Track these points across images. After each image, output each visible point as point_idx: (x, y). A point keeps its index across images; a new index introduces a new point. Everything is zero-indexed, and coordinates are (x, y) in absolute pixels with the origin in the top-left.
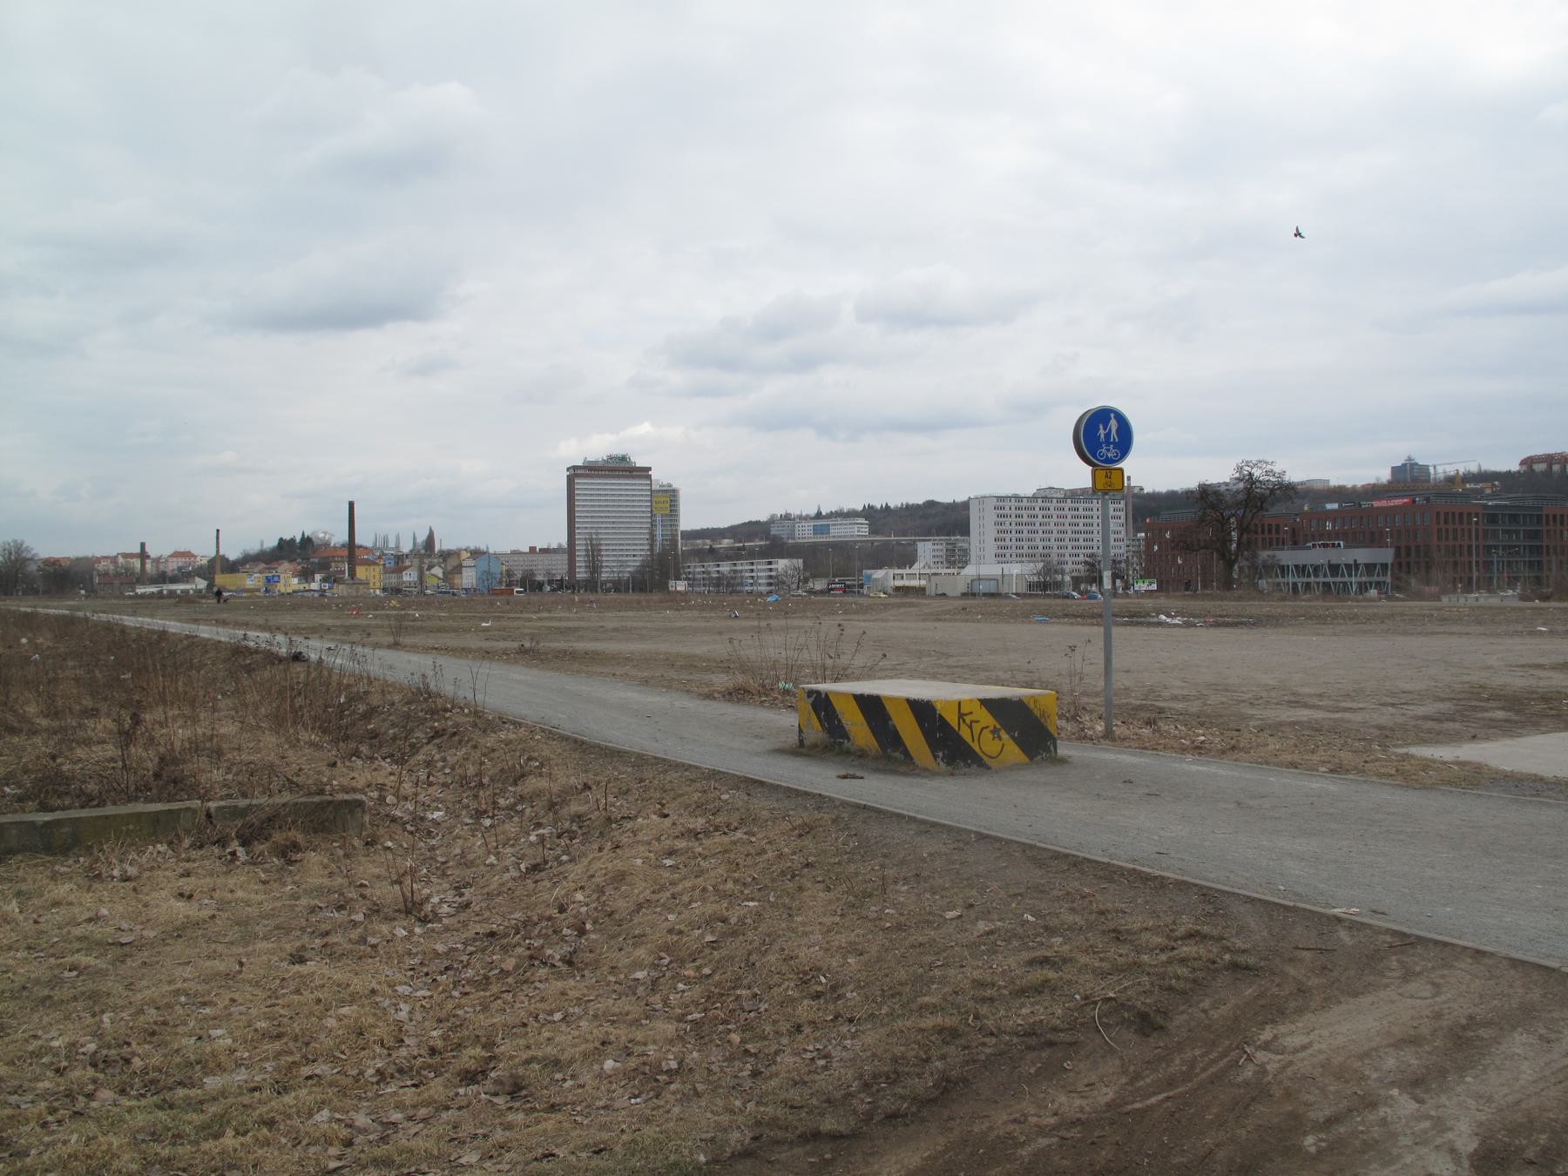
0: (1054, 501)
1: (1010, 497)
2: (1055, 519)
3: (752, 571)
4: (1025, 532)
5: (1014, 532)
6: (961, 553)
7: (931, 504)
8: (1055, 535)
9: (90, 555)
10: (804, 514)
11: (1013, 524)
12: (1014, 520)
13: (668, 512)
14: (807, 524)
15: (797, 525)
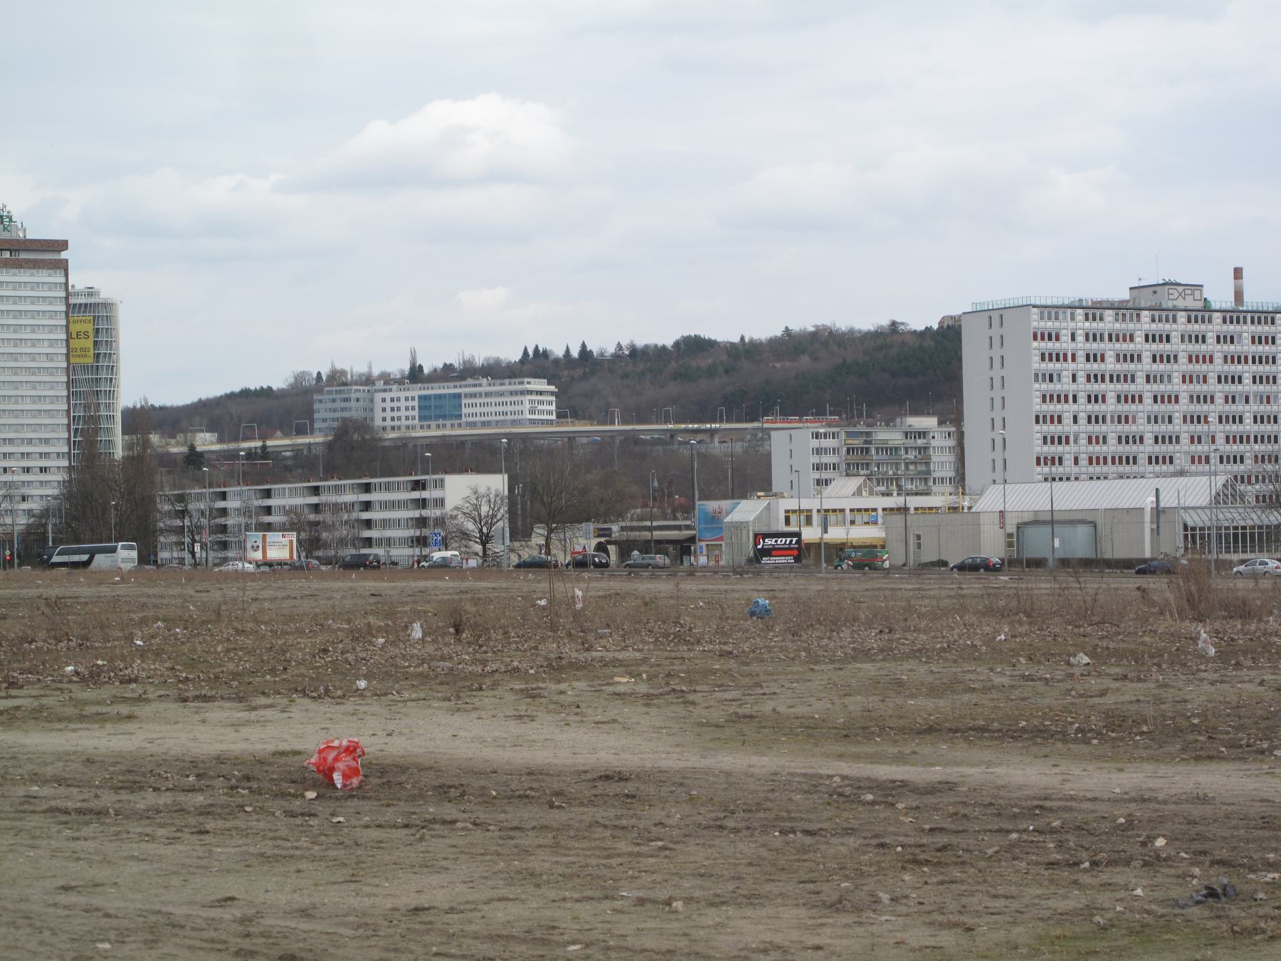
0: (1182, 317)
1: (1072, 307)
2: (1183, 366)
3: (367, 506)
4: (1111, 399)
5: (1082, 399)
6: (883, 457)
7: (693, 346)
8: (1184, 406)
9: (736, 340)
10: (376, 372)
11: (1081, 379)
12: (1082, 366)
13: (90, 360)
14: (403, 395)
15: (379, 396)
